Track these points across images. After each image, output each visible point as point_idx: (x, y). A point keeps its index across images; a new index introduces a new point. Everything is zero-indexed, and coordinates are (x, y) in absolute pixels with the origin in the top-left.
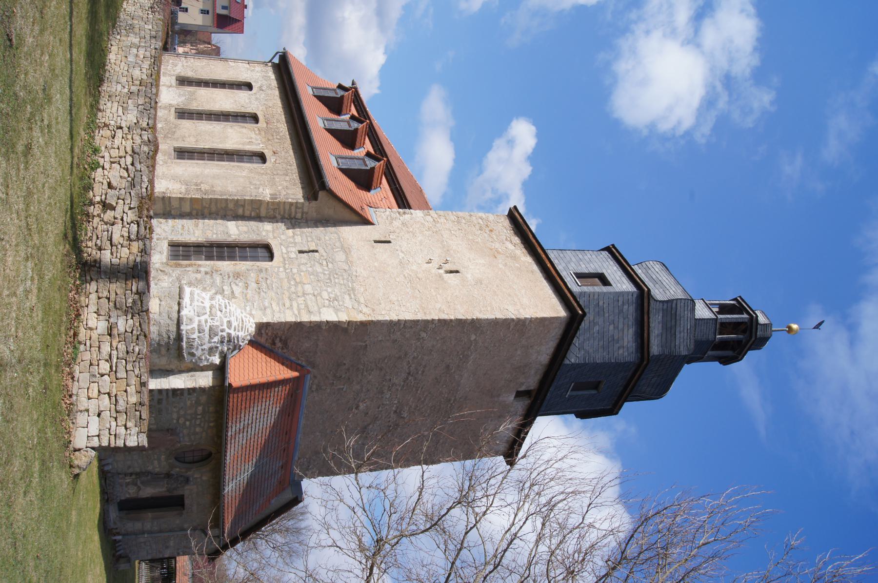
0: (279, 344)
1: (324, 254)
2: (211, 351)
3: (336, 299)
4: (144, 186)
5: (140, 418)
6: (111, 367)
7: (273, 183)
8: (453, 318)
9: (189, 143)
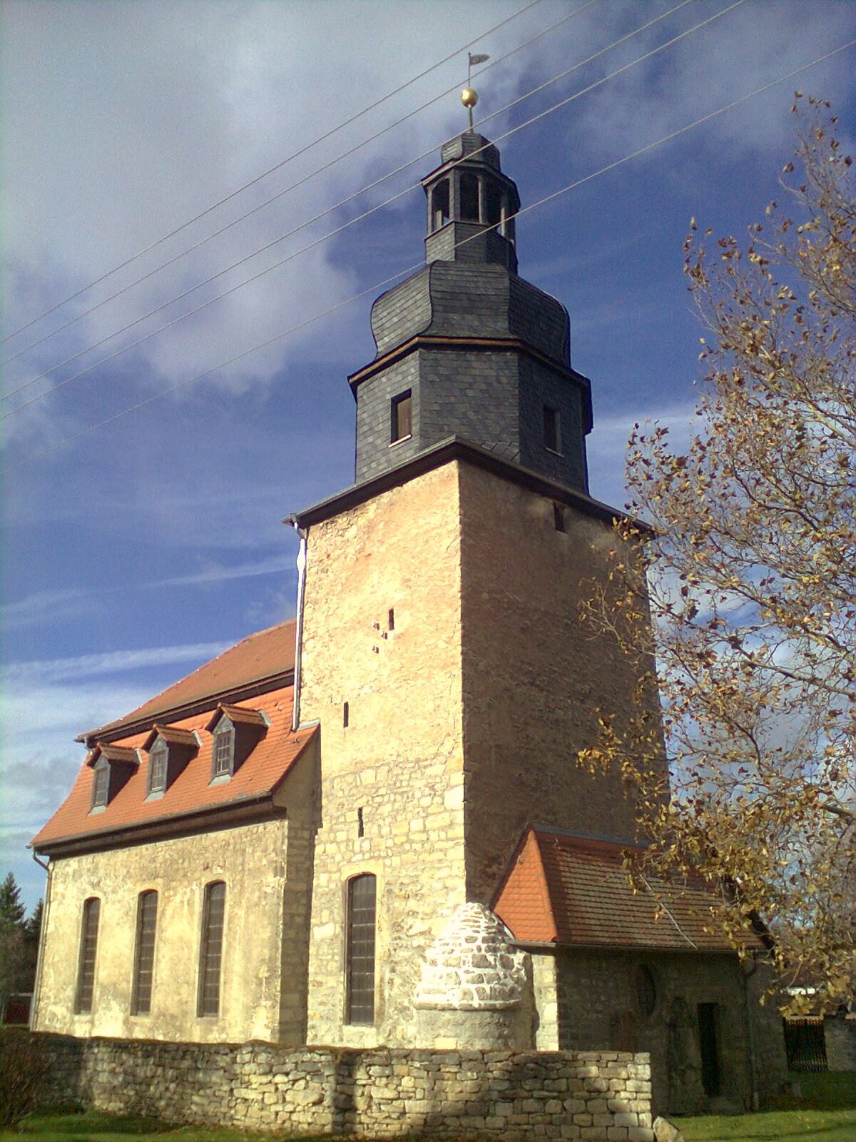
0: (495, 868)
1: (365, 799)
2: (507, 965)
3: (432, 788)
4: (317, 1058)
5: (616, 1061)
6: (554, 1098)
7: (259, 871)
8: (459, 626)
9: (191, 997)
